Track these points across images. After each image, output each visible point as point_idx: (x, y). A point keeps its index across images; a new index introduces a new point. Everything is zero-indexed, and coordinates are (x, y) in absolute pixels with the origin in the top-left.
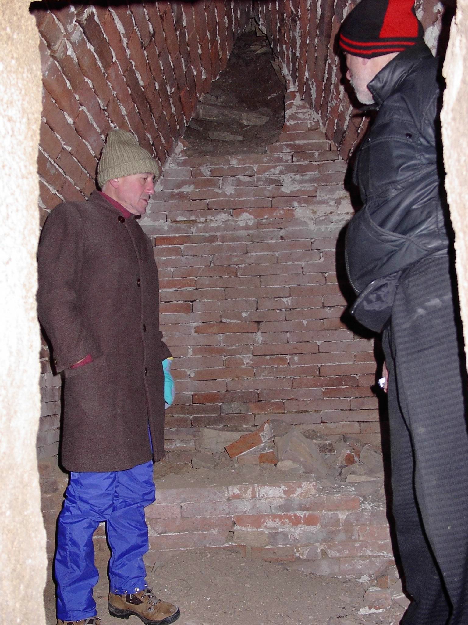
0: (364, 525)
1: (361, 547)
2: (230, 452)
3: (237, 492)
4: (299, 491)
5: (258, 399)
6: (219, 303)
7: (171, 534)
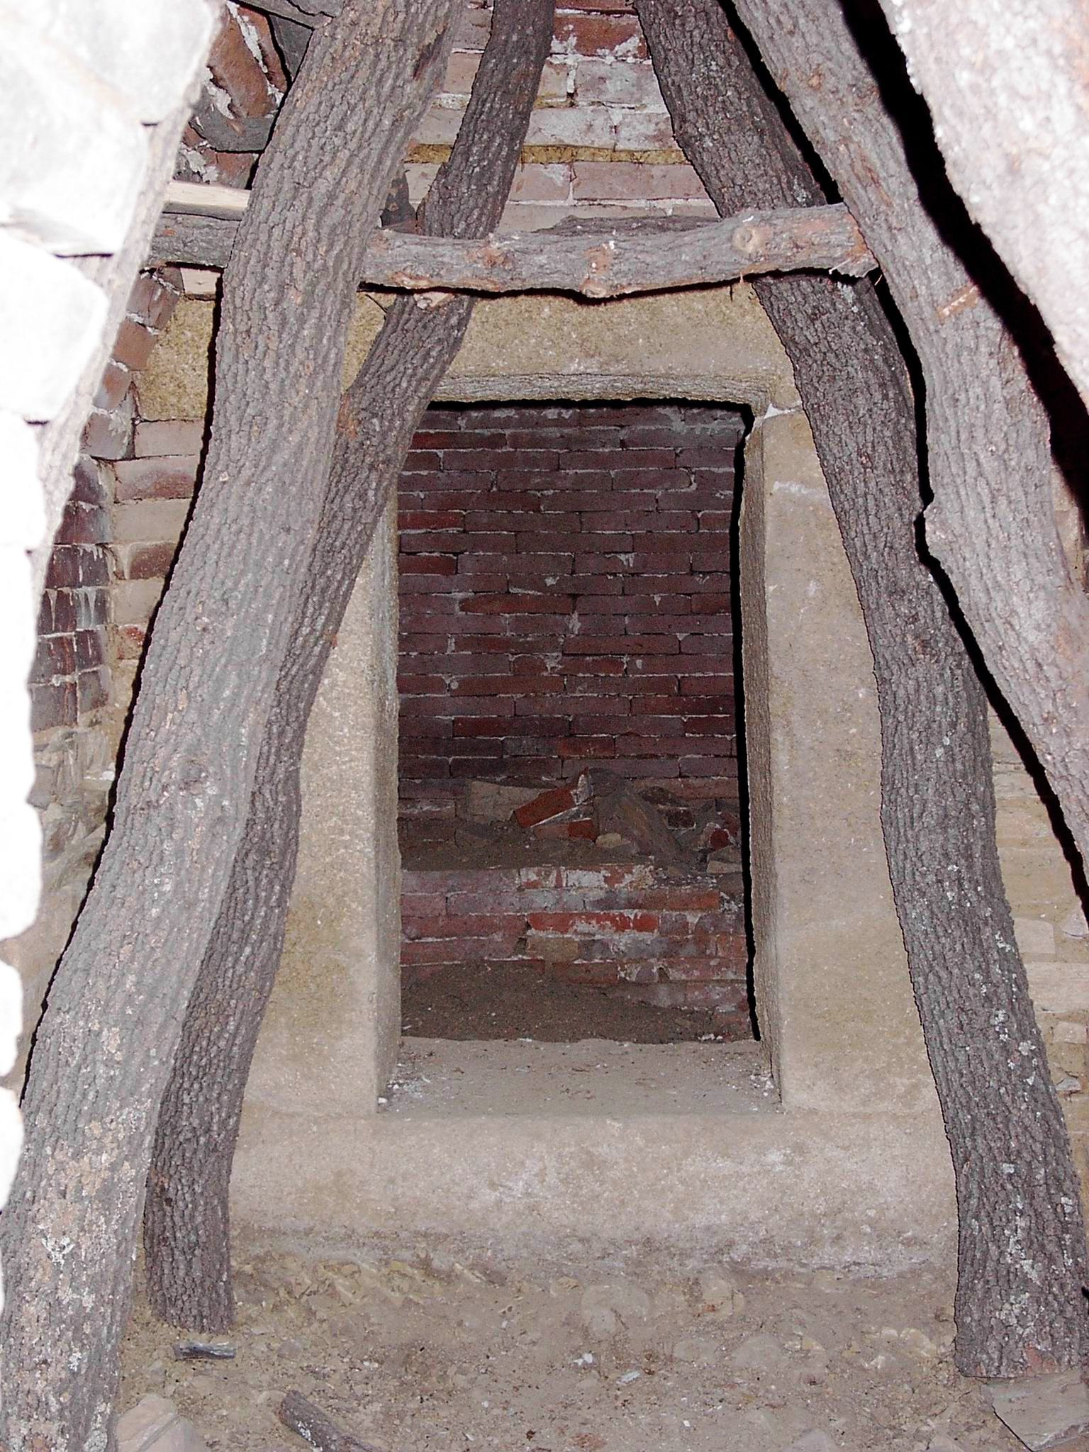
0: (725, 933)
1: (719, 966)
2: (525, 817)
3: (533, 877)
4: (628, 878)
5: (567, 733)
6: (505, 558)
7: (430, 940)
